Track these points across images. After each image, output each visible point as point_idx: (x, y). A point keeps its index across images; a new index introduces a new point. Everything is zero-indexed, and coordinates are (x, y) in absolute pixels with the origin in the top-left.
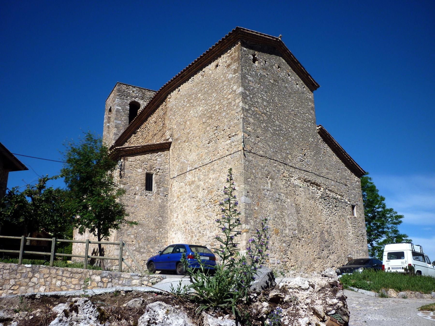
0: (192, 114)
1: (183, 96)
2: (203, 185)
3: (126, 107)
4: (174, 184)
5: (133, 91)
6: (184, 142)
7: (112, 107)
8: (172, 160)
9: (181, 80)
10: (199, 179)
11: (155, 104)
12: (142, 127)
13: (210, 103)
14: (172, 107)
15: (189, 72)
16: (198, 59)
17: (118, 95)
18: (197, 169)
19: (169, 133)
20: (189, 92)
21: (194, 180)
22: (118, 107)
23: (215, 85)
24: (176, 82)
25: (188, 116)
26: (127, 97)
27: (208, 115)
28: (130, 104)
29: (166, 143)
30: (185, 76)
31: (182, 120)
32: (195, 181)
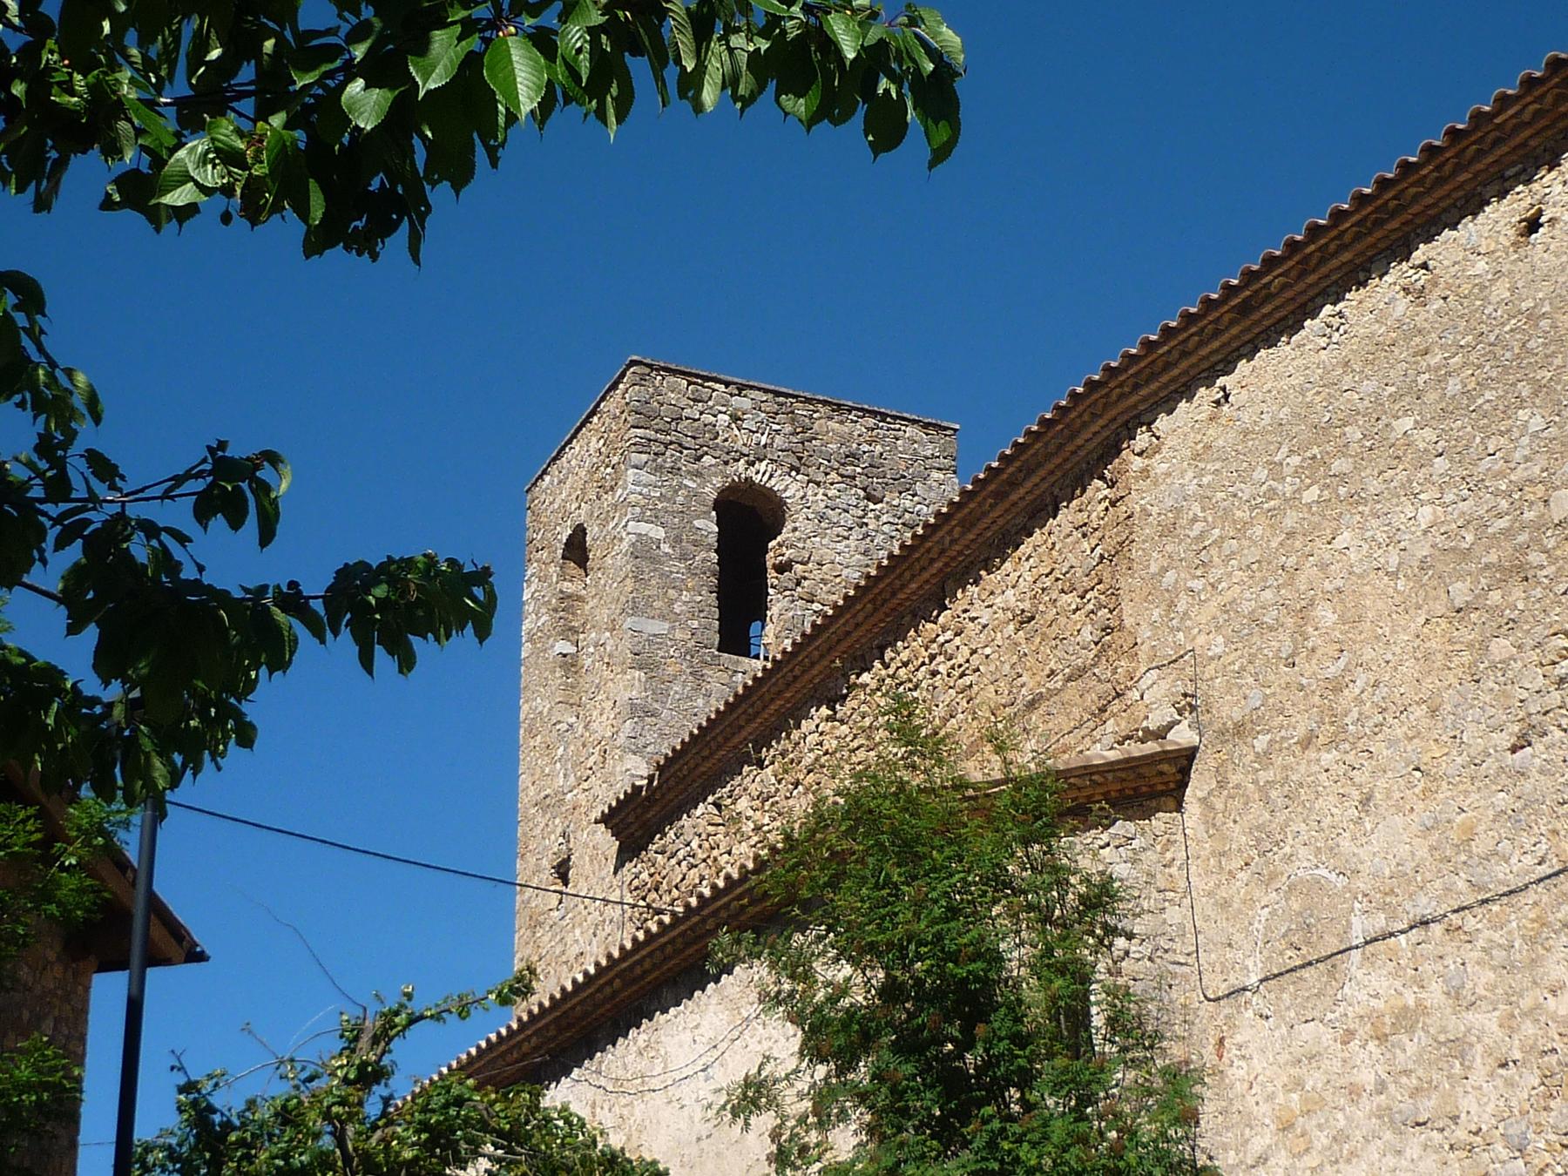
0: (1353, 555)
1: (1264, 432)
2: (1500, 1034)
3: (697, 523)
4: (1239, 1038)
5: (735, 418)
6: (1306, 743)
7: (592, 531)
8: (1210, 873)
9: (1234, 331)
10: (1455, 994)
11: (1014, 497)
12: (905, 656)
13: (1500, 475)
14: (1178, 511)
15: (1302, 275)
16: (1383, 184)
17: (643, 446)
18: (1437, 929)
19: (1164, 685)
20: (1310, 405)
21: (1411, 1003)
22: (644, 528)
23: (1530, 352)
24: (1201, 344)
25: (1323, 567)
26: (699, 459)
27: (1493, 558)
28: (717, 505)
29: (1165, 756)
30: (1270, 297)
31: (1268, 595)
32: (1422, 1009)
